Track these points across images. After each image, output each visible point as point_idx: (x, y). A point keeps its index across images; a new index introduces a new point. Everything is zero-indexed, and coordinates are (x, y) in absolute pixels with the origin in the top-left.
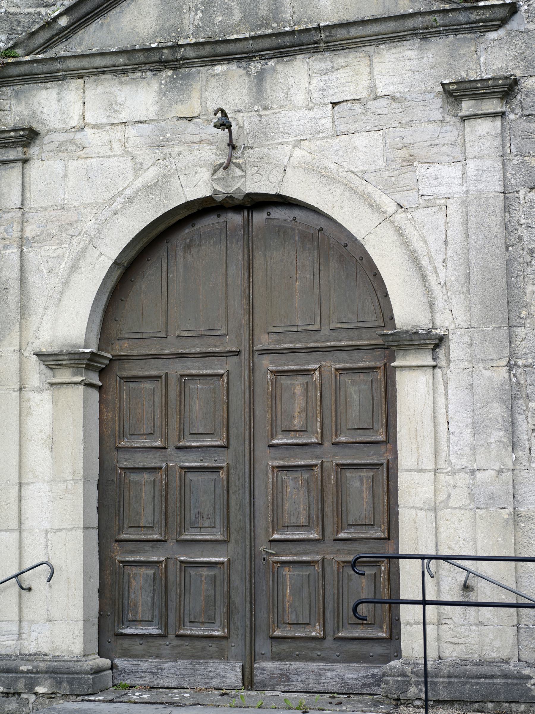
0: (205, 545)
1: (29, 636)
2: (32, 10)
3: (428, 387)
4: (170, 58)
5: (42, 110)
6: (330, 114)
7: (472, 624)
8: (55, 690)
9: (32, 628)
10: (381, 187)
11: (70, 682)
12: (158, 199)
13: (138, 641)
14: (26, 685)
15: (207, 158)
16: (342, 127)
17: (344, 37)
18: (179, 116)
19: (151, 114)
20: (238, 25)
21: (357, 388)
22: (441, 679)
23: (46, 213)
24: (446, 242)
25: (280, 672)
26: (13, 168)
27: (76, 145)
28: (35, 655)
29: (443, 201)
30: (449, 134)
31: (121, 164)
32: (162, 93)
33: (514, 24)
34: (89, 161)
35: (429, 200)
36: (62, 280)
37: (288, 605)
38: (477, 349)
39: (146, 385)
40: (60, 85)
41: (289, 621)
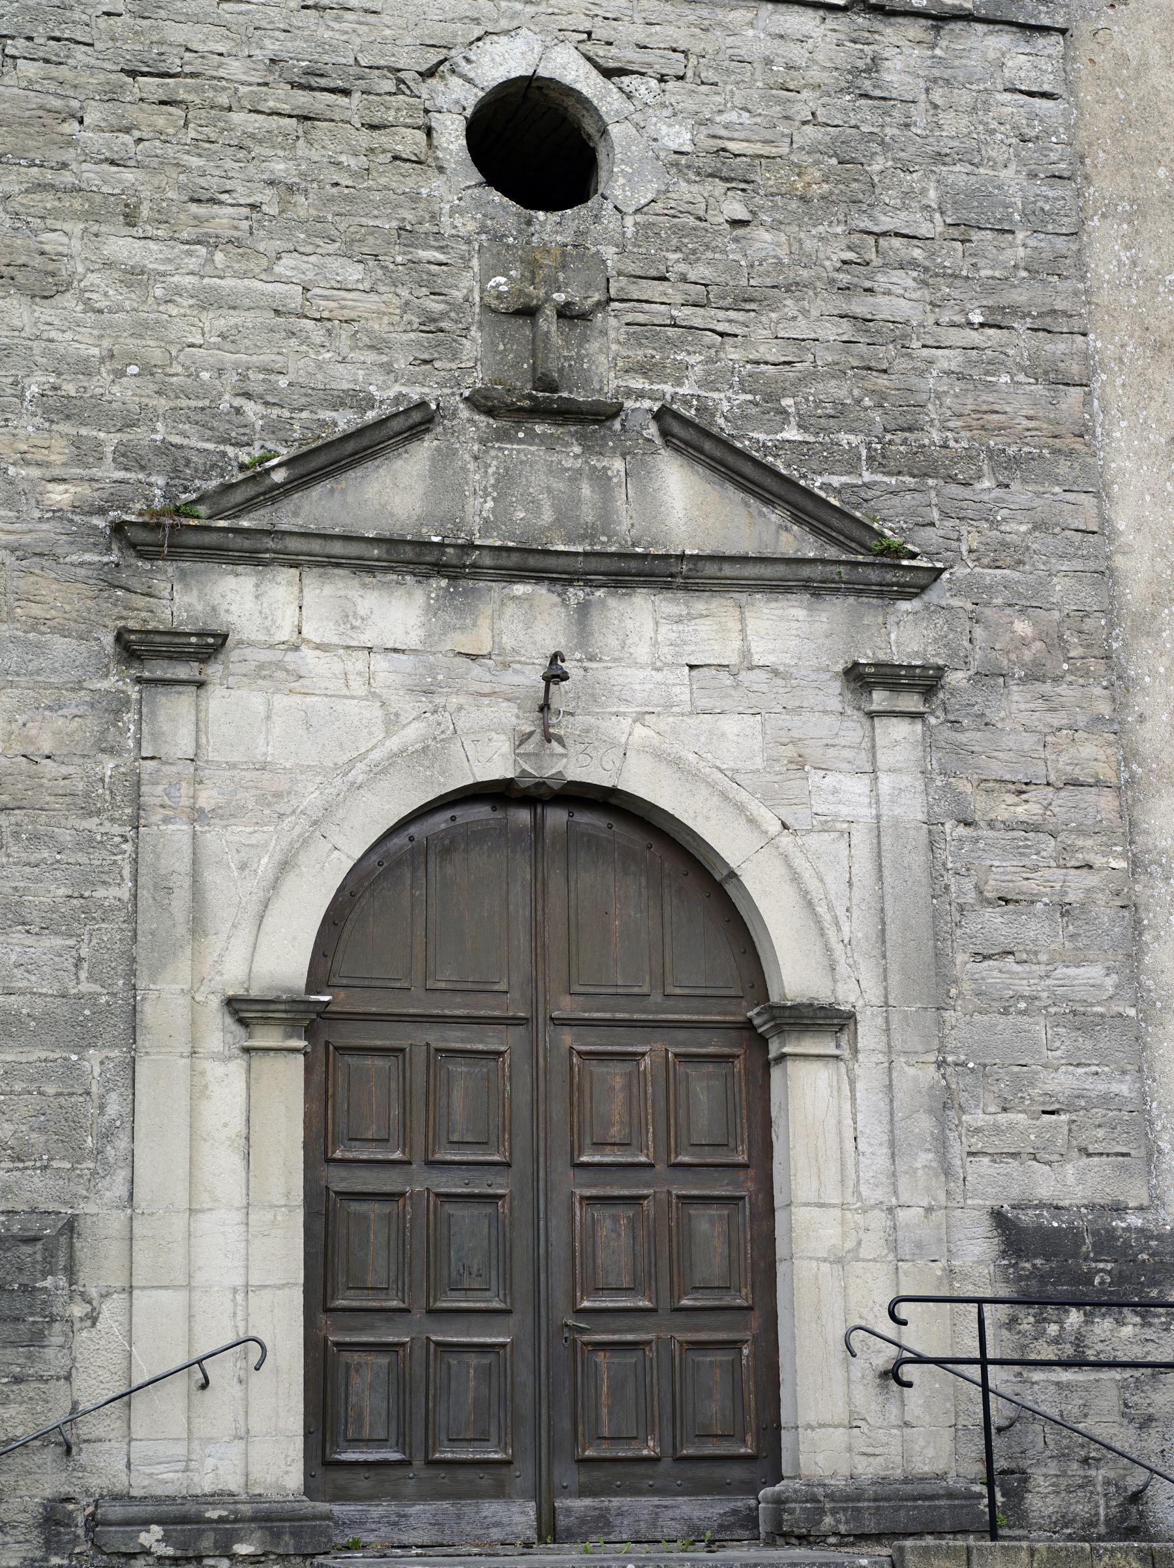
0: (474, 1318)
1: (202, 1464)
2: (210, 446)
3: (831, 1087)
4: (455, 561)
5: (227, 607)
6: (686, 681)
7: (893, 1427)
8: (269, 1549)
9: (207, 1451)
10: (758, 795)
11: (296, 1534)
12: (428, 773)
13: (363, 1473)
14: (216, 1542)
15: (504, 721)
16: (704, 703)
17: (713, 575)
18: (458, 650)
19: (413, 639)
20: (549, 529)
21: (705, 1084)
22: (866, 1504)
23: (235, 772)
24: (850, 883)
25: (596, 1513)
26: (180, 693)
27: (287, 671)
28: (212, 1496)
29: (845, 825)
30: (851, 733)
31: (363, 711)
32: (431, 611)
33: (933, 595)
34: (308, 699)
35: (826, 822)
36: (264, 884)
37: (605, 1411)
38: (897, 1036)
39: (376, 1062)
40: (260, 572)
41: (606, 1435)
